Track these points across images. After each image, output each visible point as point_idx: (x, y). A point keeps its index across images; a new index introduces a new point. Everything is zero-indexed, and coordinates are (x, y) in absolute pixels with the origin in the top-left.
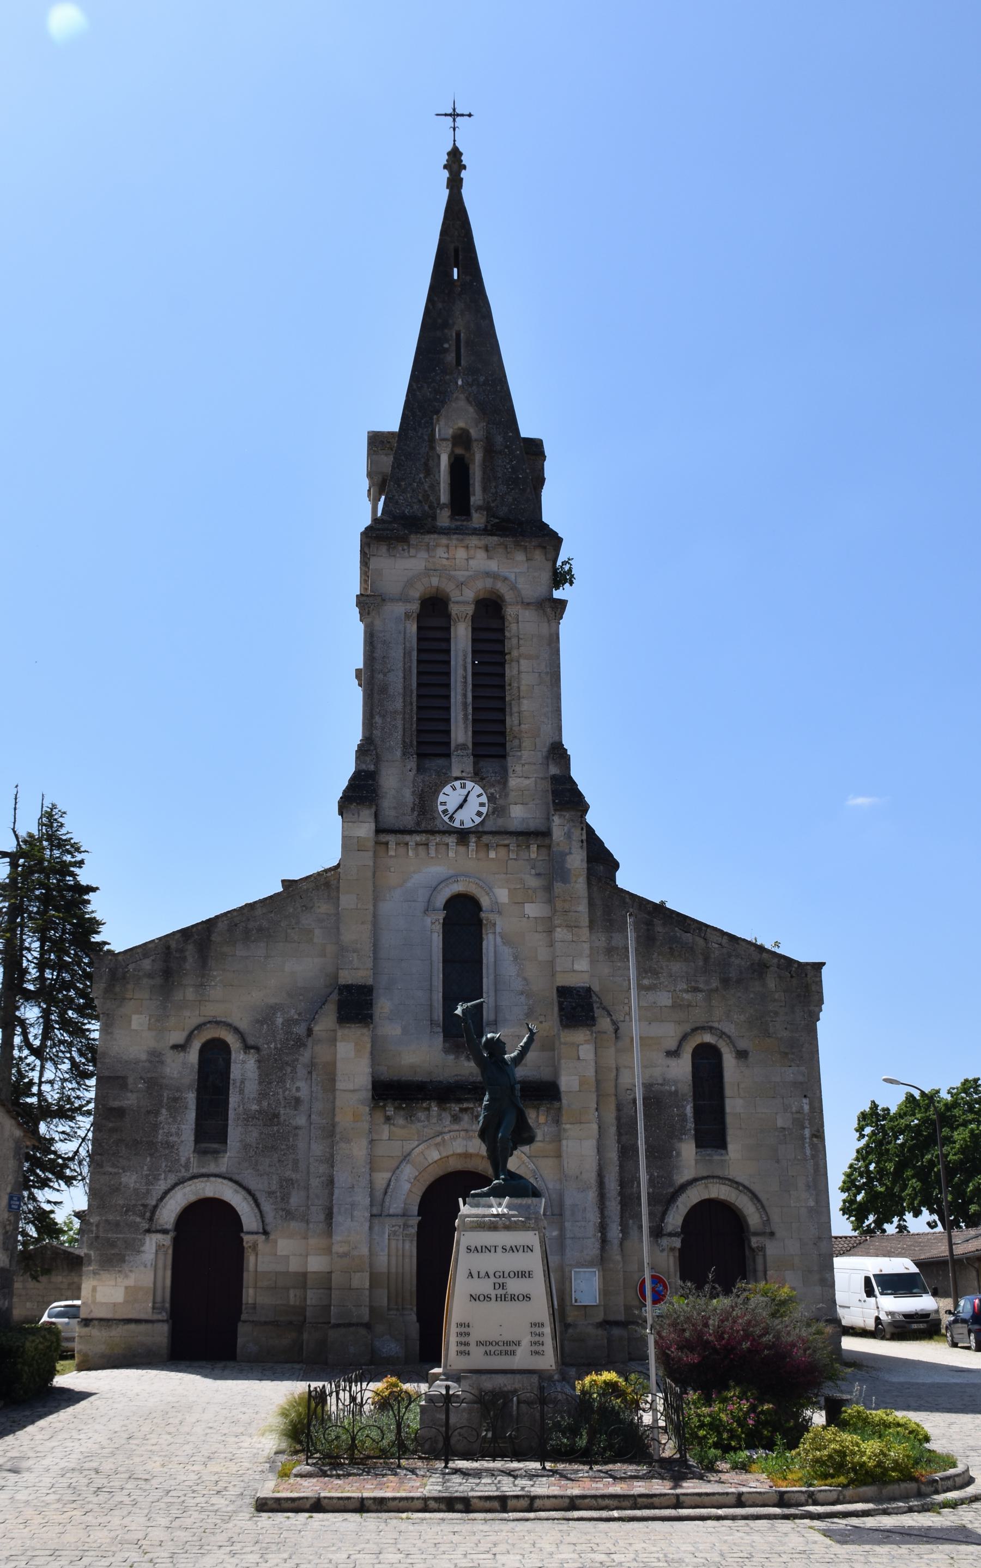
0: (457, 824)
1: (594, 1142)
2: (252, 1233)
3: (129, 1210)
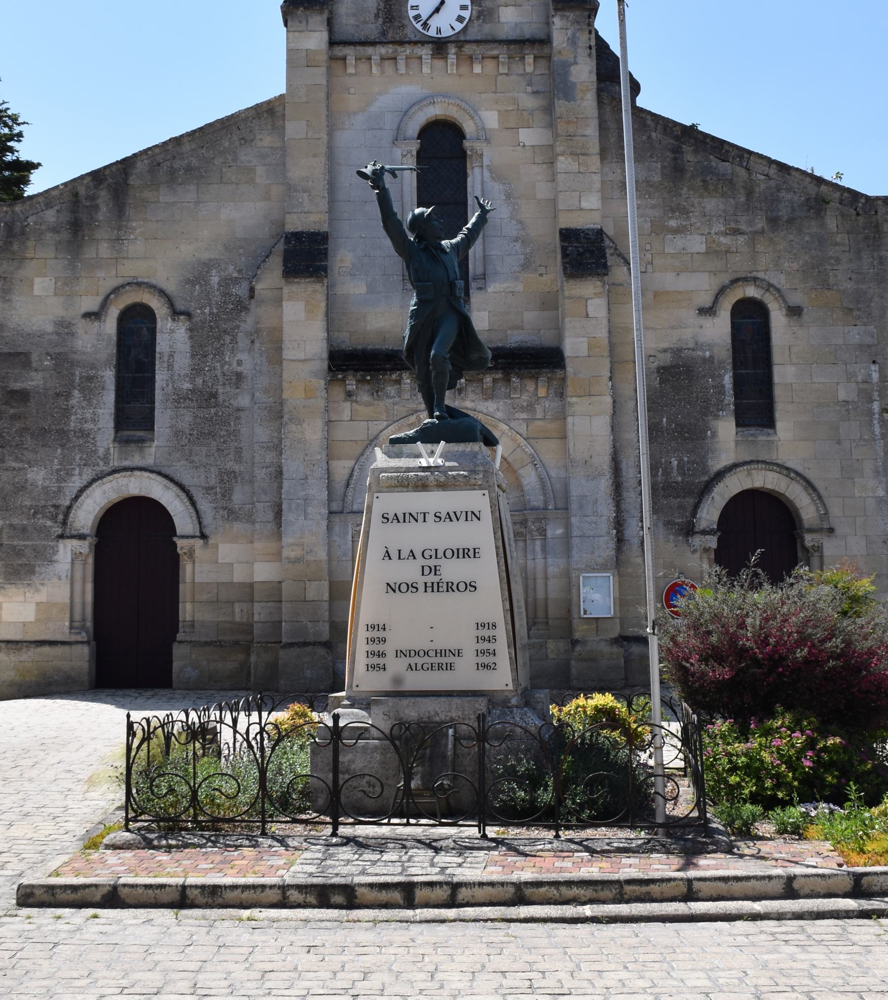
0: (432, 33)
1: (608, 419)
2: (187, 537)
3: (37, 511)
